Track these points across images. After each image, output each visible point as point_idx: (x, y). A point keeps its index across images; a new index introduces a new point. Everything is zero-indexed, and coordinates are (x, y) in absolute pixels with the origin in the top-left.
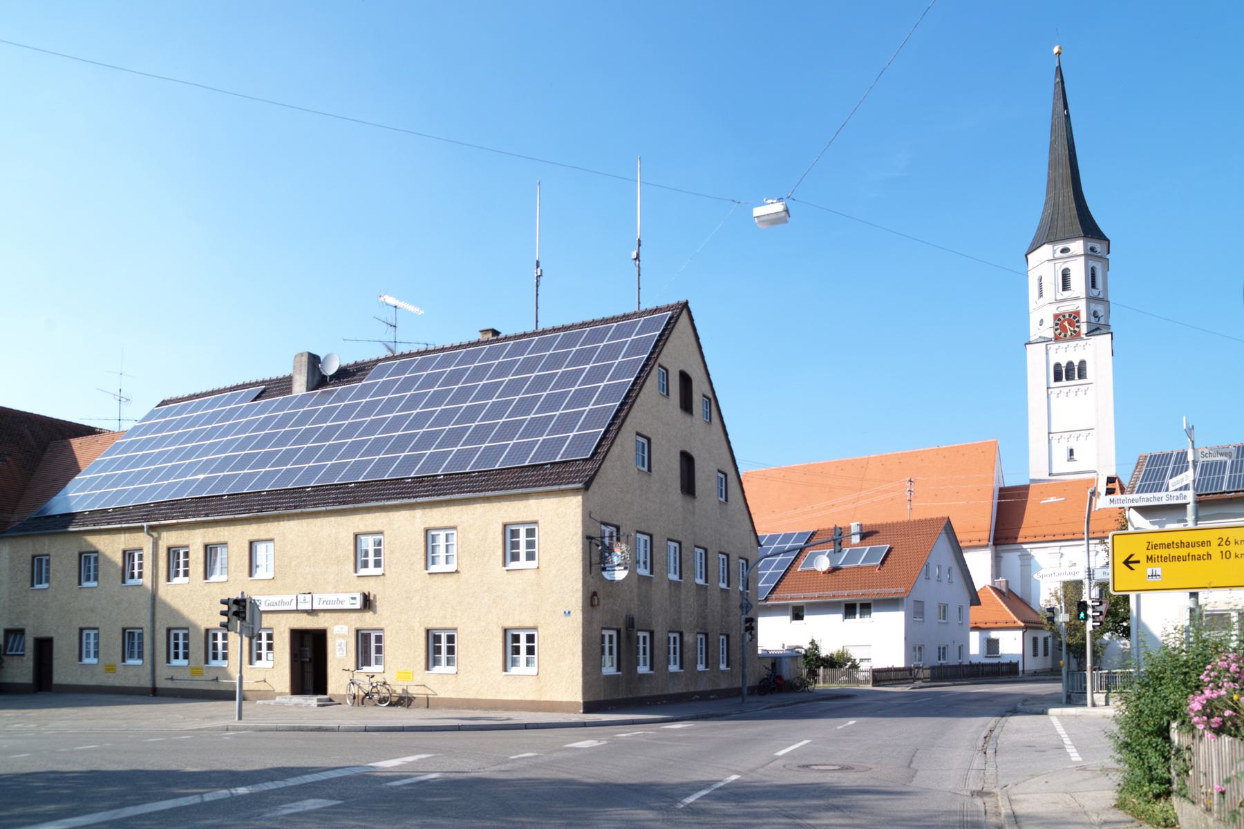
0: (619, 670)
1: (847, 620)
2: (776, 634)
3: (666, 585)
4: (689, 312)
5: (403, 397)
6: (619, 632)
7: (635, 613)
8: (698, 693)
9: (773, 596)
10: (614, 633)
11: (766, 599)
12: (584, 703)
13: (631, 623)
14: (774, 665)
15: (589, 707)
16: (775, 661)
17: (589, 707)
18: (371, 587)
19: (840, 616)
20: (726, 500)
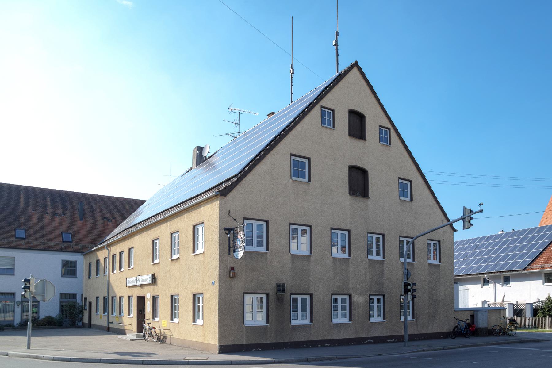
0: (268, 322)
1: (504, 287)
2: (473, 297)
3: (329, 262)
4: (360, 69)
5: (537, 236)
6: (268, 295)
7: (287, 280)
8: (371, 338)
9: (533, 266)
10: (264, 297)
11: (525, 269)
12: (220, 346)
13: (281, 289)
14: (472, 316)
15: (224, 349)
16: (474, 313)
17: (224, 349)
18: (155, 270)
19: (541, 282)
20: (412, 199)
